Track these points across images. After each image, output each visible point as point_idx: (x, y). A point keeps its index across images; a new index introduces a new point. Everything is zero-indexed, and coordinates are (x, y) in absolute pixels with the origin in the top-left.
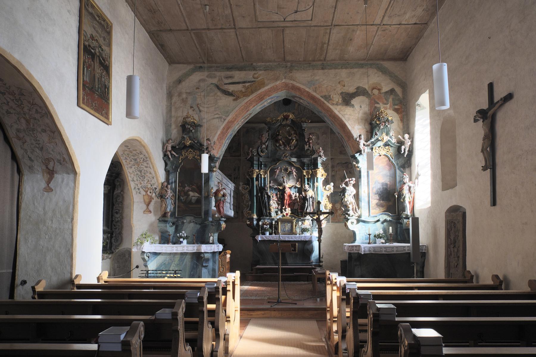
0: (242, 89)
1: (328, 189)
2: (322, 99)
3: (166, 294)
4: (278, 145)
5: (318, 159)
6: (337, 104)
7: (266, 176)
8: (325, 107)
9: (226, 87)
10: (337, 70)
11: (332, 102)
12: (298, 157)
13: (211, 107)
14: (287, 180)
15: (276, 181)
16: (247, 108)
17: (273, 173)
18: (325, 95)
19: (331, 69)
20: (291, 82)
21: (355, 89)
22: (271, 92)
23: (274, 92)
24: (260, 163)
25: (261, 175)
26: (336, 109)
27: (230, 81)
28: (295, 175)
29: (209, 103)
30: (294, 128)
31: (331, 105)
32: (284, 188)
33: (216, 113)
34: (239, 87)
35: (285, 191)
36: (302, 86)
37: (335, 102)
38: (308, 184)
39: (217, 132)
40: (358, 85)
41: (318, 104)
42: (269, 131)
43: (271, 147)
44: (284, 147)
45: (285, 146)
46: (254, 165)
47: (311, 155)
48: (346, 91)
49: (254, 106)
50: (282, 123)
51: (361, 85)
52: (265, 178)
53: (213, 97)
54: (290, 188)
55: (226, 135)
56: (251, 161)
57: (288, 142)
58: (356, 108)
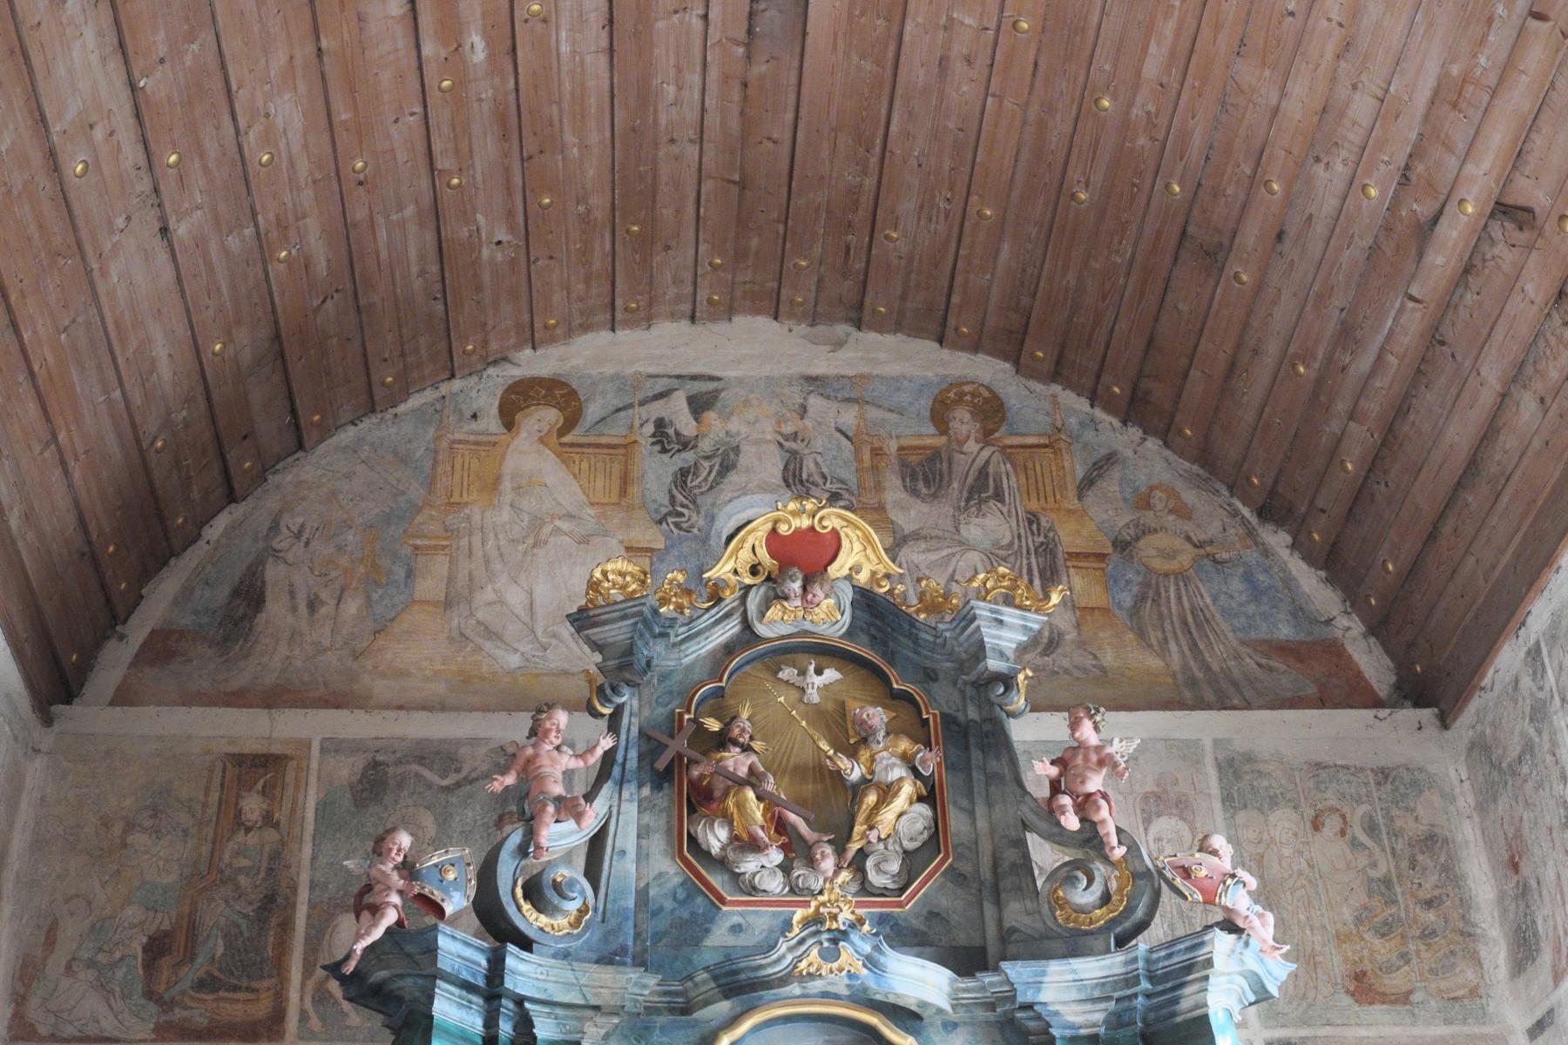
3: (1488, 653)
42: (615, 690)
43: (642, 856)
45: (797, 851)
47: (1112, 923)
50: (762, 630)
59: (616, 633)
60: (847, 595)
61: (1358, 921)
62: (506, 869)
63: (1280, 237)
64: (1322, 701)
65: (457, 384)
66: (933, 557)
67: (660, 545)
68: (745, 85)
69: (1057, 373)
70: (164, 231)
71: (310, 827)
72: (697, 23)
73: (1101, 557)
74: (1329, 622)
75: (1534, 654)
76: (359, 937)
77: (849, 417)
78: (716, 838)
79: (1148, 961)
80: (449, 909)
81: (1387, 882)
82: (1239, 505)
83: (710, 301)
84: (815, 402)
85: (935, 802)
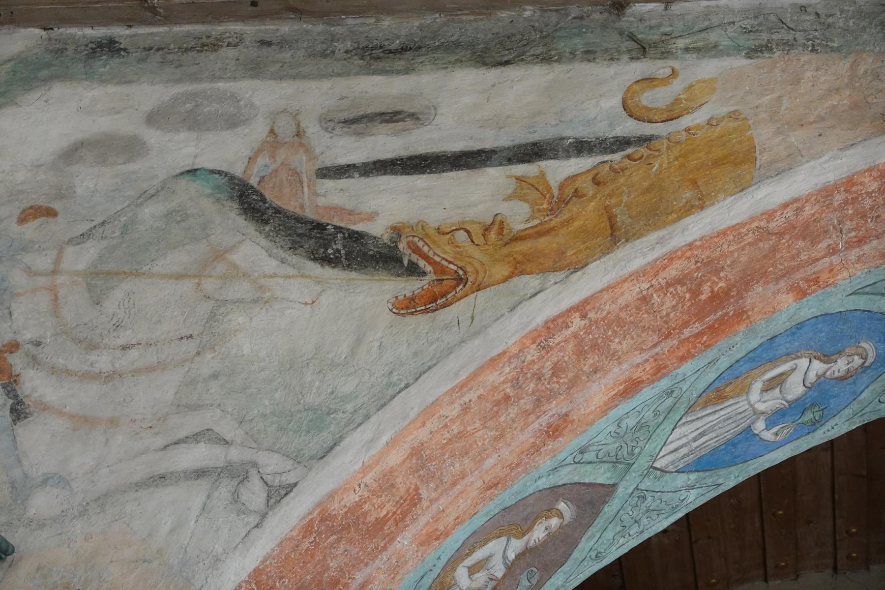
9: (336, 200)
16: (552, 395)
22: (823, 245)
23: (861, 241)
33: (193, 423)
49: (631, 387)
53: (187, 286)
83: (849, 557)
85: (781, 374)
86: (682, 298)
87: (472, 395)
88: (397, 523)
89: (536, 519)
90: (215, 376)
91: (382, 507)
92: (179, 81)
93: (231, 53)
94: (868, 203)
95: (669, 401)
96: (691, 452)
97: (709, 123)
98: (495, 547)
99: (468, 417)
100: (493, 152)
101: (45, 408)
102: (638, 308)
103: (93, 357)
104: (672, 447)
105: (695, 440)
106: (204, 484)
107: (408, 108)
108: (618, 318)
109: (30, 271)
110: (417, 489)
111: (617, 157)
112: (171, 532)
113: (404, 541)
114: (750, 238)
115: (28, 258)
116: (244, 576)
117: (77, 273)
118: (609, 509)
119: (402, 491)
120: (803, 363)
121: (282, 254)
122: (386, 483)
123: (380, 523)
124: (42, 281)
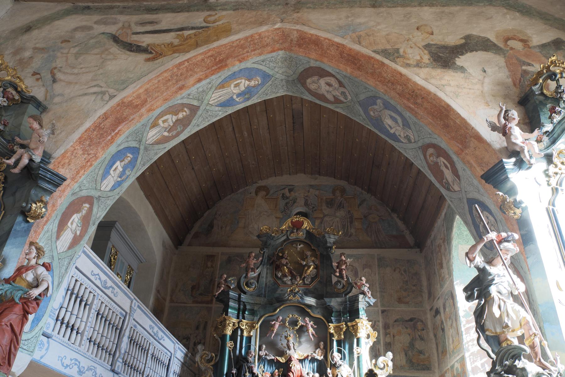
0: (173, 40)
1: (382, 366)
2: (378, 57)
4: (279, 276)
5: (360, 300)
6: (418, 65)
7: (252, 334)
8: (385, 75)
9: (135, 39)
10: (409, 9)
11: (405, 61)
12: (319, 297)
13: (87, 72)
14: (296, 344)
15: (273, 346)
16: (180, 80)
17: (266, 328)
18: (383, 48)
19: (393, 7)
20: (298, 27)
21: (462, 38)
22: (245, 50)
23: (254, 50)
24: (242, 307)
25: (242, 331)
26: (418, 75)
27: (149, 28)
28: (313, 335)
29: (82, 66)
30: (312, 246)
31: (401, 66)
32: (289, 360)
33: (95, 83)
34: (169, 38)
35: (291, 368)
36: (322, 35)
37: (411, 62)
38: (339, 351)
39: (82, 124)
40: (468, 32)
41: (367, 73)
43: (266, 278)
44: (291, 280)
45: (293, 277)
46: (229, 310)
47: (344, 292)
48: (438, 43)
49: (200, 80)
50: (290, 238)
51: (475, 33)
52: (249, 338)
53: (99, 56)
54: (301, 361)
55: (112, 138)
56: (224, 300)
57: (299, 270)
58: (473, 74)
59: (264, 239)
60: (305, 232)
61: (401, 288)
62: (242, 280)
63: (389, 164)
64: (400, 247)
65: (248, 187)
66: (330, 219)
67: (282, 217)
68: (294, 137)
69: (355, 184)
70: (193, 168)
71: (218, 268)
72: (284, 128)
73: (361, 219)
74: (403, 231)
75: (432, 242)
76: (217, 292)
77: (317, 193)
78: (280, 274)
79: (349, 299)
80: (232, 288)
81: (407, 281)
82: (388, 209)
84: (311, 190)
85: (238, 83)
86: (212, 60)
87: (160, 78)
88: (141, 106)
89: (179, 111)
90: (102, 74)
91: (137, 102)
92: (103, 15)
93: (116, 9)
94: (256, 41)
95: (210, 86)
96: (218, 101)
97: (222, 24)
98: (168, 117)
99: (159, 83)
100: (173, 29)
101: (61, 80)
102: (201, 62)
103: (73, 70)
104: (213, 99)
105: (219, 98)
106: (95, 95)
107: (155, 21)
108: (196, 63)
109: (62, 53)
110: (146, 99)
111: (200, 30)
112: (86, 105)
113: (143, 110)
114: (228, 47)
115: (62, 51)
116: (102, 114)
117: (73, 53)
118: (199, 113)
119: (143, 99)
120: (243, 81)
121: (121, 50)
122: (139, 97)
123: (137, 106)
124: (65, 55)
